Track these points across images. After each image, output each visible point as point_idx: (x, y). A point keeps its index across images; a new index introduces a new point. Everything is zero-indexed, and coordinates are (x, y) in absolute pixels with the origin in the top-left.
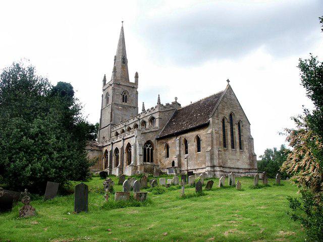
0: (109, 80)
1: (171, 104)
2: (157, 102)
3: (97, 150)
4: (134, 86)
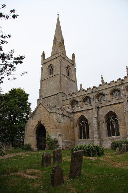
0: (48, 55)
1: (97, 86)
2: (101, 81)
3: (67, 116)
4: (73, 63)
